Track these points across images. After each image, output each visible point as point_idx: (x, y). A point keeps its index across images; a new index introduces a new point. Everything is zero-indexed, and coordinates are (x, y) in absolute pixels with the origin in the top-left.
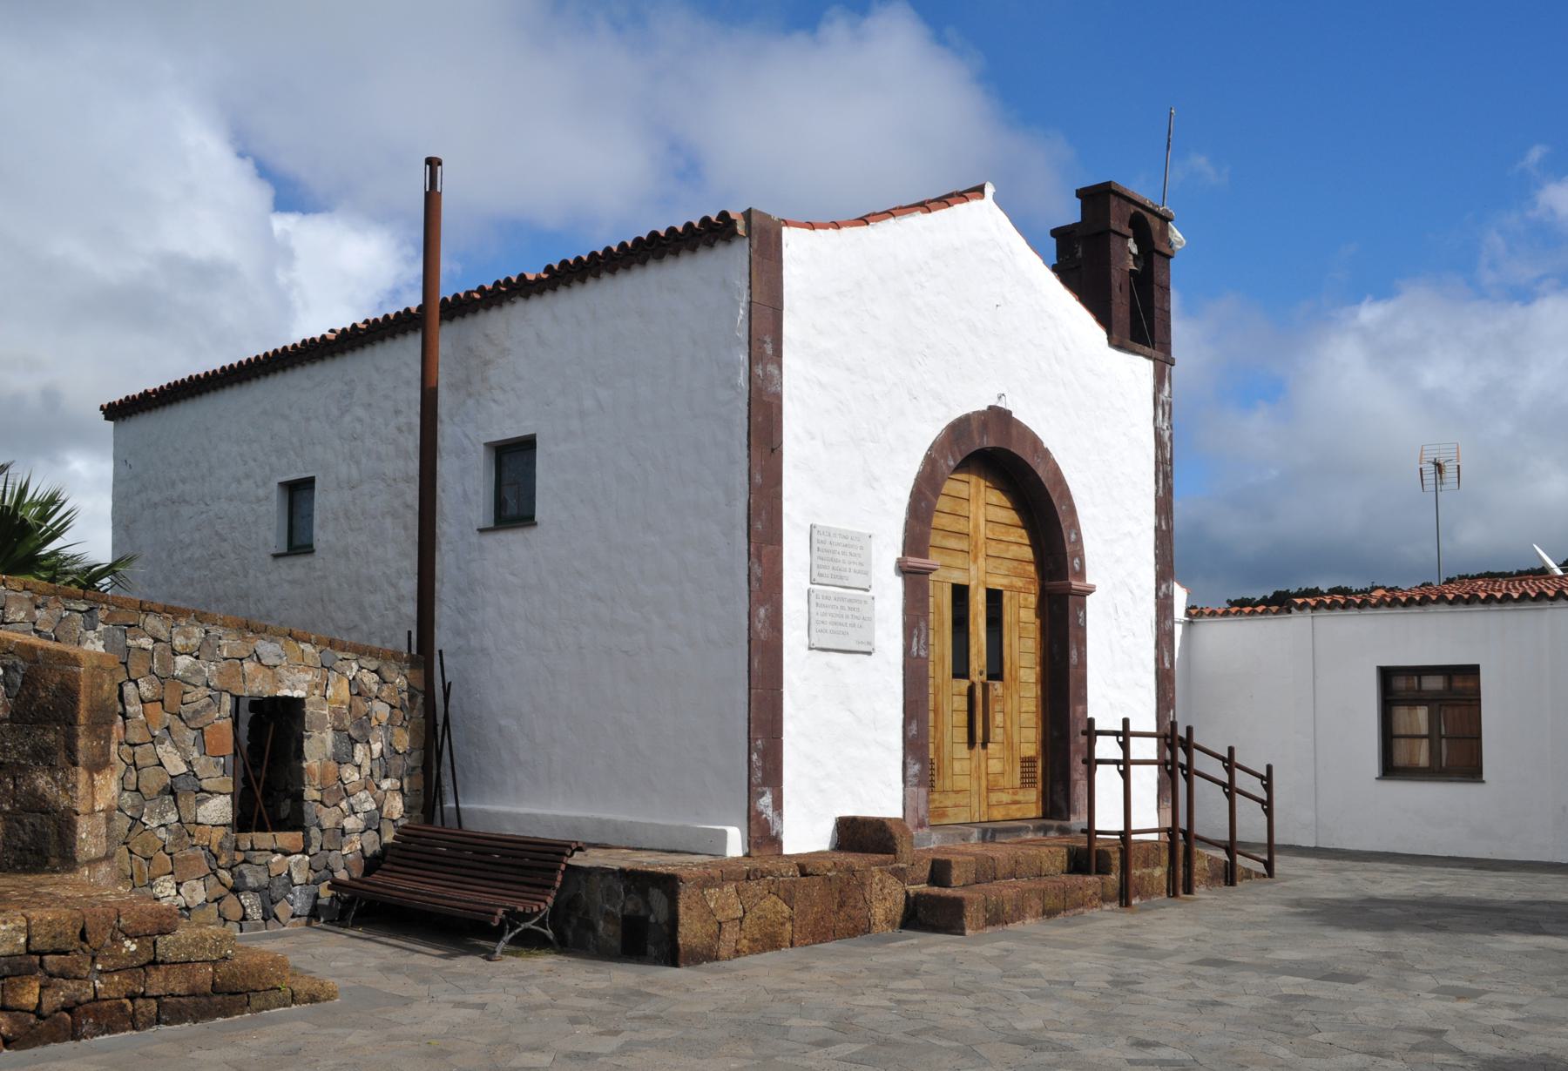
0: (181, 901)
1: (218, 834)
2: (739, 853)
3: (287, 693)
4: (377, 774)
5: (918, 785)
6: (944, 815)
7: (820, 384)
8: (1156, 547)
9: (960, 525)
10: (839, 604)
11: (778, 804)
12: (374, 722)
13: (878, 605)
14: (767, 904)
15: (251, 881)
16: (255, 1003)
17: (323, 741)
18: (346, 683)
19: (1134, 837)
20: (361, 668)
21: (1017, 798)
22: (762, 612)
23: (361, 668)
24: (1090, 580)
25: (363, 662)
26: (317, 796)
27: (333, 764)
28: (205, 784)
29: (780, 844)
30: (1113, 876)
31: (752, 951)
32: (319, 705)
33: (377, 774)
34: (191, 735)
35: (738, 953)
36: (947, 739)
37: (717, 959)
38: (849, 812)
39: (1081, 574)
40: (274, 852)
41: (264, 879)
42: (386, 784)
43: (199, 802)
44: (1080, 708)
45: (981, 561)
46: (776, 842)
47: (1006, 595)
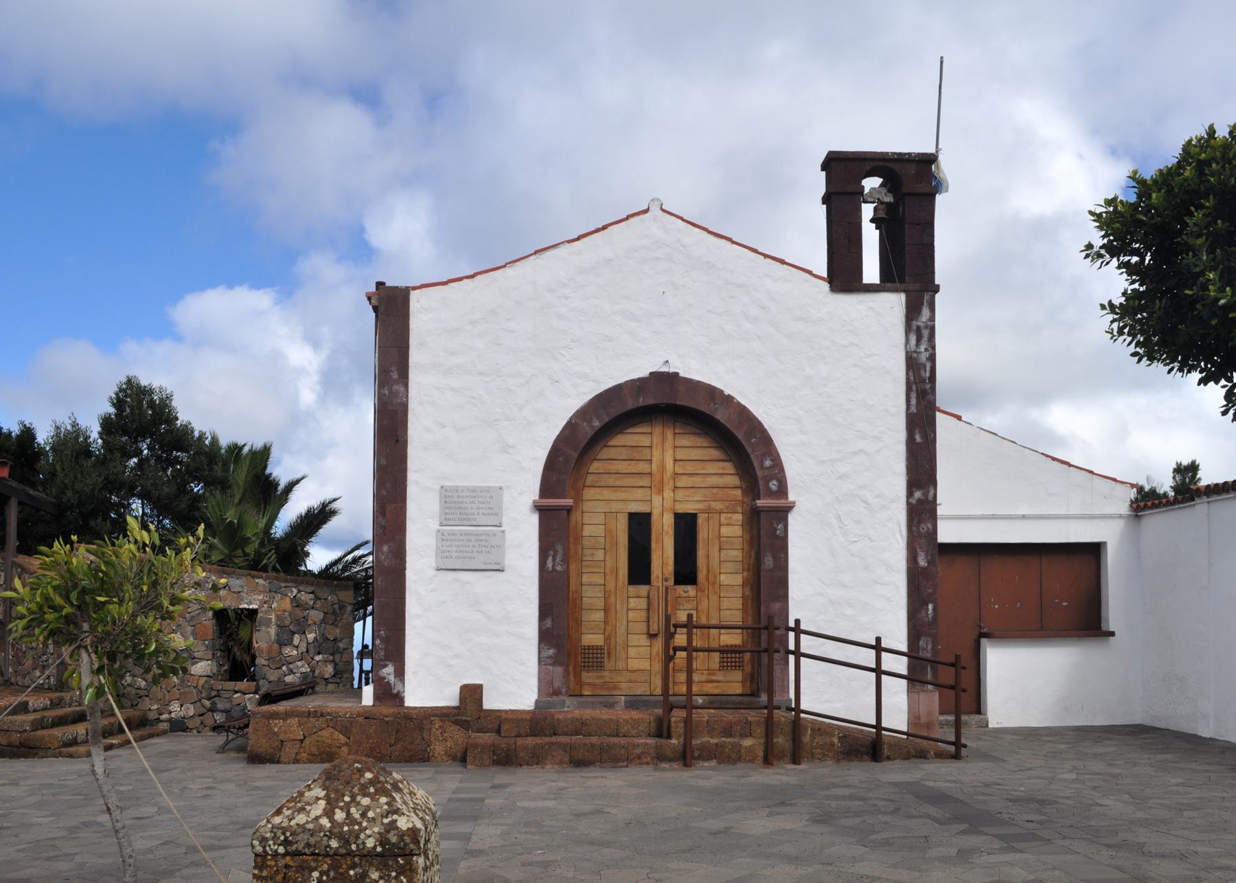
0: (182, 714)
1: (202, 681)
2: (371, 703)
3: (246, 606)
4: (312, 651)
5: (553, 664)
6: (615, 688)
7: (452, 389)
8: (908, 459)
9: (642, 467)
10: (465, 538)
11: (400, 673)
12: (310, 622)
13: (508, 536)
14: (324, 733)
15: (220, 706)
16: (41, 754)
17: (268, 633)
18: (288, 600)
19: (802, 715)
20: (299, 591)
21: (714, 678)
22: (385, 548)
23: (299, 591)
24: (791, 497)
25: (301, 588)
26: (265, 663)
27: (276, 646)
28: (196, 654)
29: (402, 700)
30: (674, 741)
31: (310, 762)
32: (267, 612)
33: (312, 651)
34: (189, 629)
35: (296, 761)
36: (621, 630)
37: (278, 762)
38: (466, 682)
39: (783, 491)
40: (236, 692)
41: (228, 706)
42: (318, 658)
43: (193, 664)
44: (777, 606)
45: (668, 494)
46: (399, 698)
47: (701, 520)
